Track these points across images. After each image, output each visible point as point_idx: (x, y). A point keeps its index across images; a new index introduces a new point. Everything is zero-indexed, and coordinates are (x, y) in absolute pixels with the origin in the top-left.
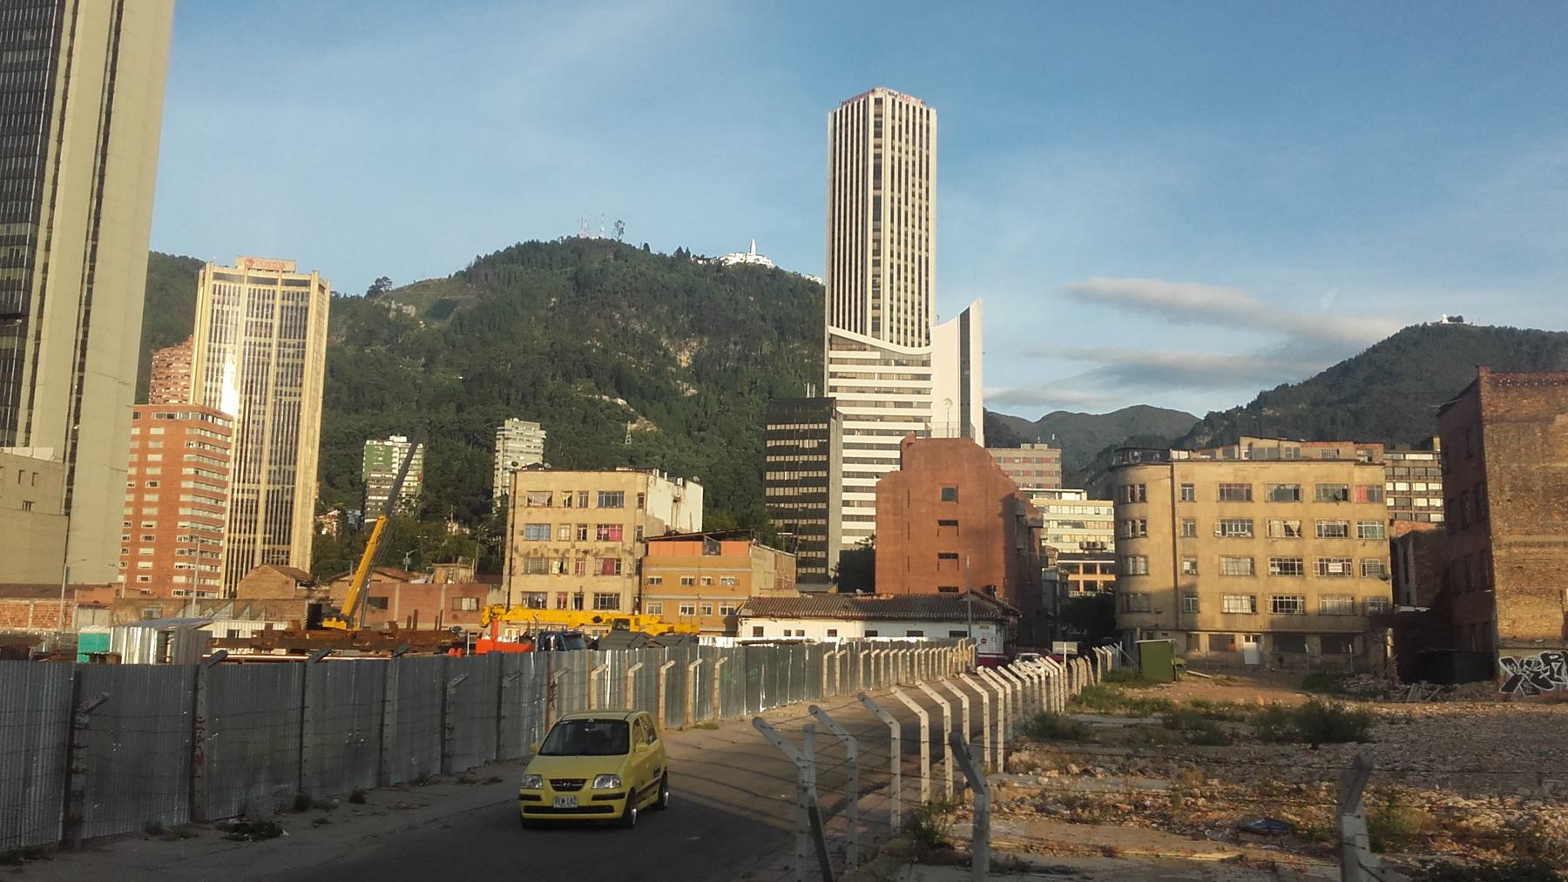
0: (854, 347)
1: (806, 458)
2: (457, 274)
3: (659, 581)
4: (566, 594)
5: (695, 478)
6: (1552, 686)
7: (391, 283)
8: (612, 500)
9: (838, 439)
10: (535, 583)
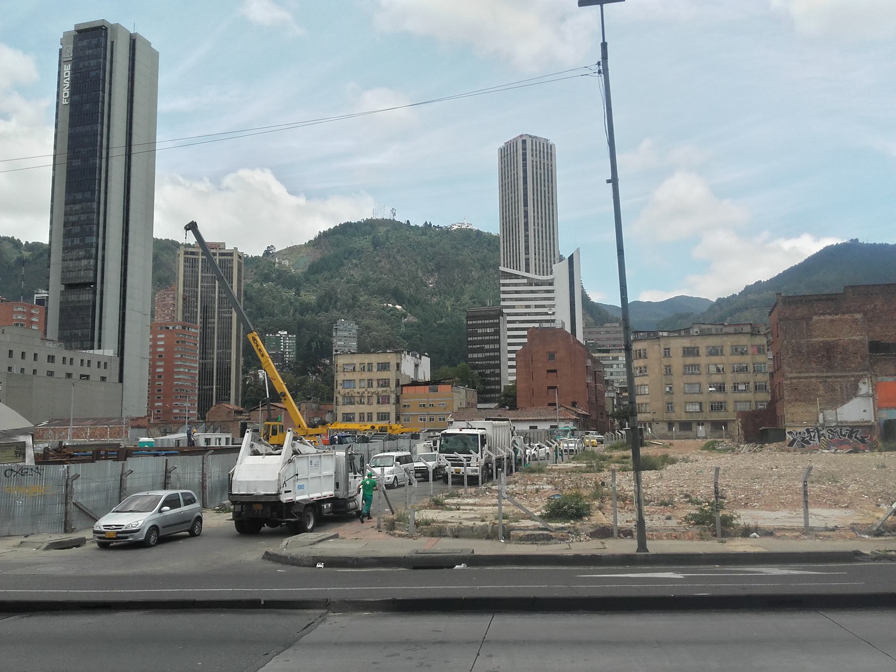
0: (513, 277)
2: (309, 242)
3: (408, 406)
4: (363, 413)
5: (426, 354)
6: (811, 444)
7: (275, 248)
8: (384, 367)
9: (504, 326)
10: (348, 409)
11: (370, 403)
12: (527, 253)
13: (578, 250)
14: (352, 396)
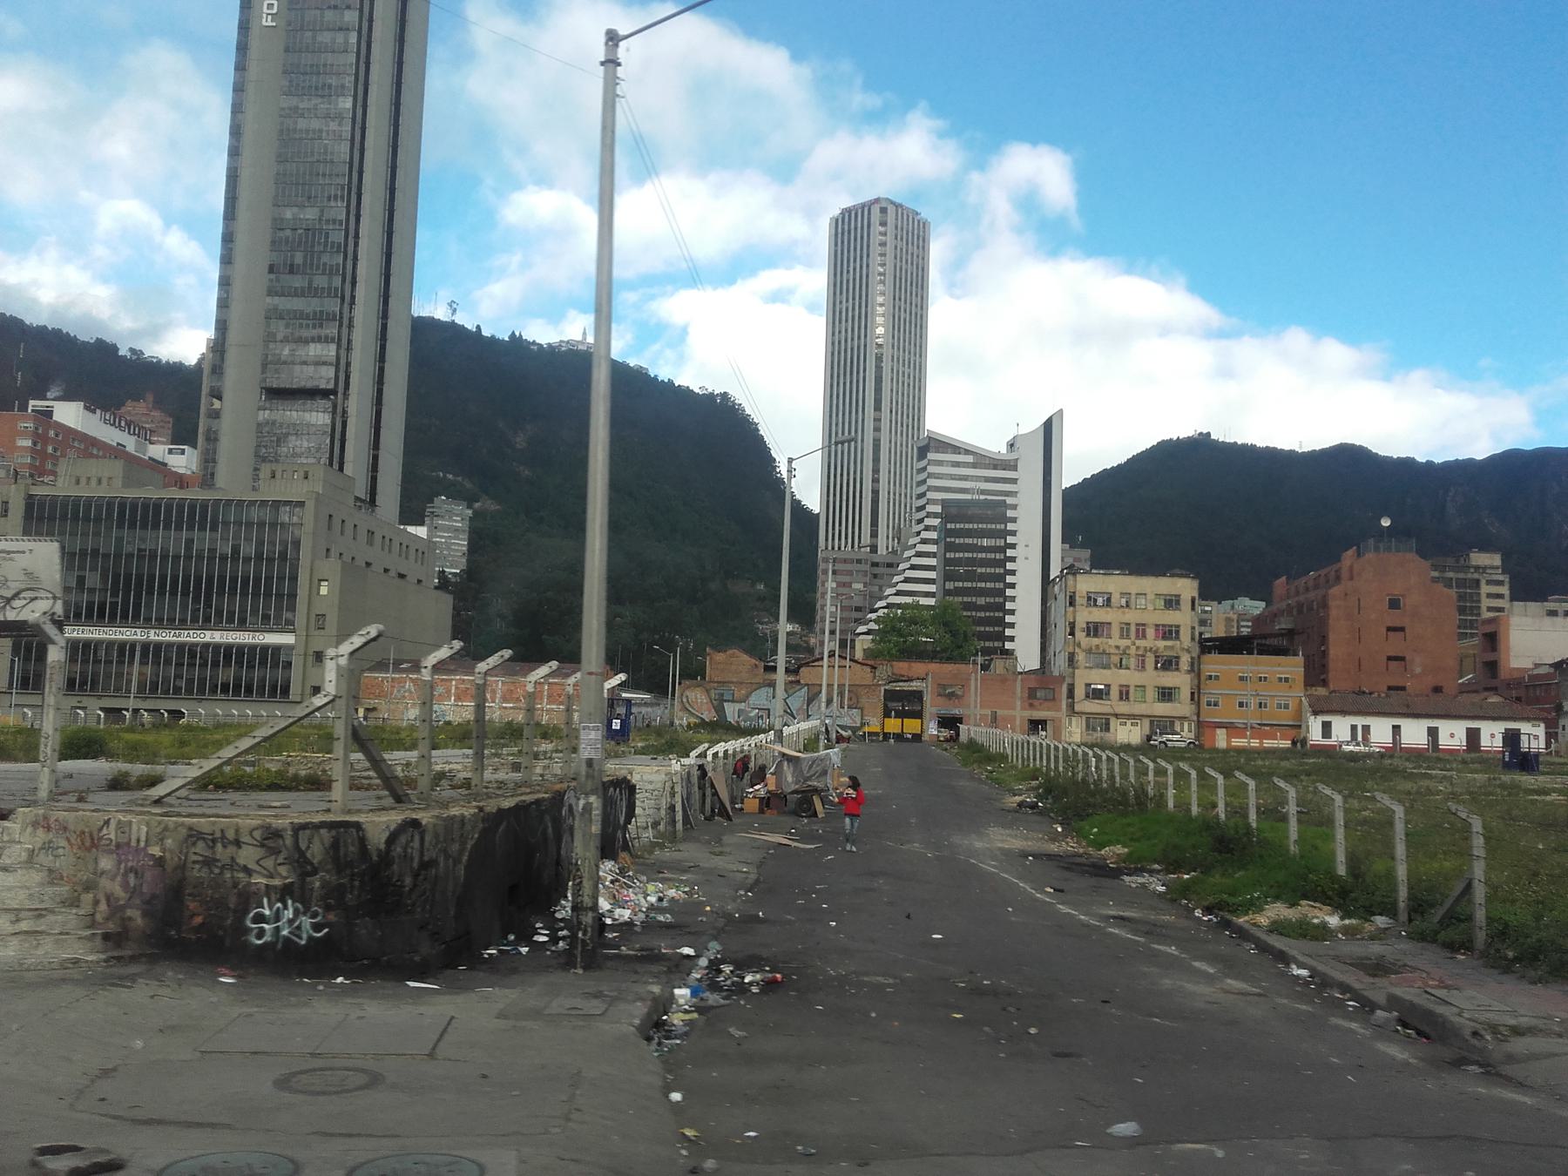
1: (984, 555)
3: (1217, 678)
11: (1142, 667)
12: (878, 408)
13: (1061, 412)
14: (1104, 652)
